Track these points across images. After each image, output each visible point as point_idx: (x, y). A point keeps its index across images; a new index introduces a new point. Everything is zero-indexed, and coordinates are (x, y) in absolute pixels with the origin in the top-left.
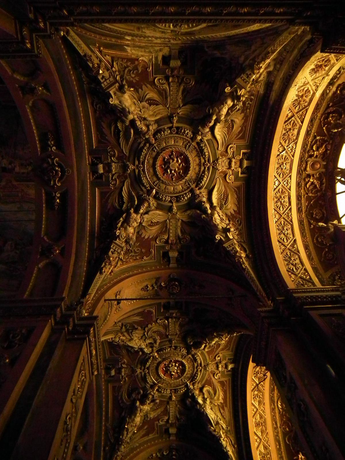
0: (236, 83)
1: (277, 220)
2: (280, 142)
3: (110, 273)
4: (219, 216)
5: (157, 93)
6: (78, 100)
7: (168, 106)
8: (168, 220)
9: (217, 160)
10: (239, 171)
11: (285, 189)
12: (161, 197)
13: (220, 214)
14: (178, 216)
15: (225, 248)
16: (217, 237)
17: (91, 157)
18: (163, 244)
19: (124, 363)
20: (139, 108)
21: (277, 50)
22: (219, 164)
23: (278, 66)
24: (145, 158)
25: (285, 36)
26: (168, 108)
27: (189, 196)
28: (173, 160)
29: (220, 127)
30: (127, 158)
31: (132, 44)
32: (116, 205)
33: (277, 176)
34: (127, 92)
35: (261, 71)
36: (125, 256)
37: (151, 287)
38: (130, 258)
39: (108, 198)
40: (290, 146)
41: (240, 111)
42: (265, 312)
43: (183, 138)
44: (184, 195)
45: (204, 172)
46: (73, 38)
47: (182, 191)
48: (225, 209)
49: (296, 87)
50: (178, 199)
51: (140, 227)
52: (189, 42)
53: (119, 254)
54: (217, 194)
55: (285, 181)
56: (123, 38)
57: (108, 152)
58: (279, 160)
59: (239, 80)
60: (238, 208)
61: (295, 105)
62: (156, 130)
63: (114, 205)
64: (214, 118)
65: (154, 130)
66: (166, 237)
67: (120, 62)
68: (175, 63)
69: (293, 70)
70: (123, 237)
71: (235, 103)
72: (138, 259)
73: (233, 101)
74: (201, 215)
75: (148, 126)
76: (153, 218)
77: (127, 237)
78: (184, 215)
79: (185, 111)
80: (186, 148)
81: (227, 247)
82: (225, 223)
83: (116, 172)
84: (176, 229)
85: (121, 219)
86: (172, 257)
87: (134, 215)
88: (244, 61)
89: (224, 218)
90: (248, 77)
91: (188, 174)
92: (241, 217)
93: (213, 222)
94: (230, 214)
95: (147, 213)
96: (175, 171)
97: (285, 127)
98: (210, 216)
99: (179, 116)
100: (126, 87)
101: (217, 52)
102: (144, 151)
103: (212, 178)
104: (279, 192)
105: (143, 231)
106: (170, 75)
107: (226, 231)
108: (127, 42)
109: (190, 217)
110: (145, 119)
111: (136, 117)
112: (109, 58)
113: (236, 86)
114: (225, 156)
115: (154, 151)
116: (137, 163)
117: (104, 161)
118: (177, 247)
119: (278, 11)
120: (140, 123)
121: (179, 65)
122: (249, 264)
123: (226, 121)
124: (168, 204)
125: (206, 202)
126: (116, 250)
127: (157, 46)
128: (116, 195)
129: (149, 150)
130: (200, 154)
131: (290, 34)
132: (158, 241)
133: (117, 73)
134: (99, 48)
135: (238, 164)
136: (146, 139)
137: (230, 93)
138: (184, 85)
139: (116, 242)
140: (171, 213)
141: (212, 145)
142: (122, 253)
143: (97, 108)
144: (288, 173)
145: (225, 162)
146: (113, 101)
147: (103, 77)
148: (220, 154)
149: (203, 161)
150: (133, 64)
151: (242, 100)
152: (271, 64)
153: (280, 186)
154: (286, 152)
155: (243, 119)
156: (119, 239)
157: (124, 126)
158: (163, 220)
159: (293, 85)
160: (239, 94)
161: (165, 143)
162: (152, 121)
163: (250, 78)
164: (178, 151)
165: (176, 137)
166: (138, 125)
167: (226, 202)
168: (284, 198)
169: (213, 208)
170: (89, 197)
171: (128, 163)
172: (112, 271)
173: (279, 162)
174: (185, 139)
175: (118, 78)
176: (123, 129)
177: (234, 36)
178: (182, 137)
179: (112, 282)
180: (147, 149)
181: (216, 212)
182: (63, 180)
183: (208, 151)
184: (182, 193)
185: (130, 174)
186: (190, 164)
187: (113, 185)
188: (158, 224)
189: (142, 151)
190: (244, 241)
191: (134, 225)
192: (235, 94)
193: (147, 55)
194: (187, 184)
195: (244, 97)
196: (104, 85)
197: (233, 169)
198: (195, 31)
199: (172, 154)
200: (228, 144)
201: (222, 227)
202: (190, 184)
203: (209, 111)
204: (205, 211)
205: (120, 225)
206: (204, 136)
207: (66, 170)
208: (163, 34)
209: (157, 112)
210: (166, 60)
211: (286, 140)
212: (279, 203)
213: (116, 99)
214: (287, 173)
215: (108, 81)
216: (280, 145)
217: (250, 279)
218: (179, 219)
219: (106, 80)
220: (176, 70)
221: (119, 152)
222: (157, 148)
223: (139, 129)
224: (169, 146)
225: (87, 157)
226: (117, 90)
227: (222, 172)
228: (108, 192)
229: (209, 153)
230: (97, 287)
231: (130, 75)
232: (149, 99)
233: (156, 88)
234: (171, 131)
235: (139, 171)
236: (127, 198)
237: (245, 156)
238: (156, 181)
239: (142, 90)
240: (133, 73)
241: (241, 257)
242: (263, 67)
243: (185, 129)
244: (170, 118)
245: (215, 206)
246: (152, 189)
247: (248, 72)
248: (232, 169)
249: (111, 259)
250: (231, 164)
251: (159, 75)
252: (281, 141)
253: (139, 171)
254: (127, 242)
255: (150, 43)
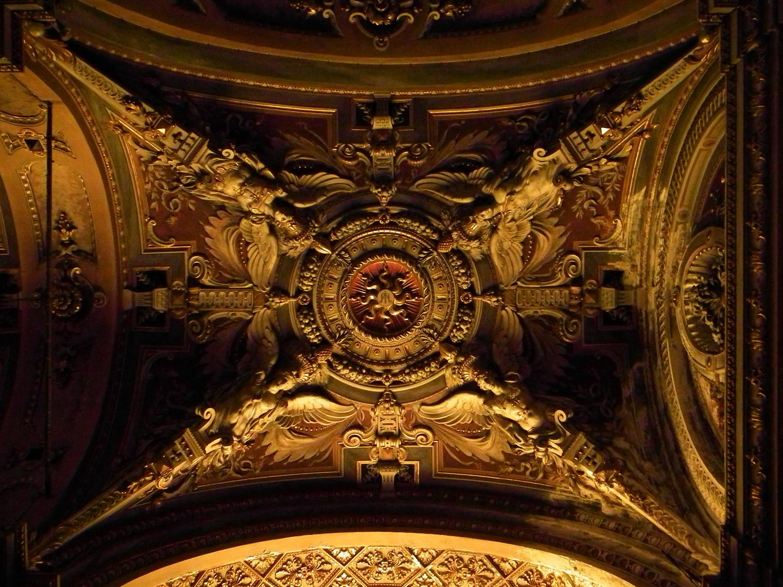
0: (574, 434)
1: (253, 564)
2: (443, 551)
3: (120, 126)
4: (262, 416)
5: (549, 260)
6: (550, 77)
7: (519, 283)
8: (250, 285)
9: (398, 404)
10: (369, 460)
11: (330, 579)
12: (311, 267)
13: (266, 418)
14: (262, 311)
15: (179, 433)
16: (208, 412)
17: (408, 102)
18: (187, 275)
19: (411, 157)
20: (520, 218)
21: (651, 515)
22: (388, 409)
23: (612, 525)
24: (407, 230)
25: (683, 528)
26: (515, 284)
27: (312, 337)
28: (398, 298)
29: (474, 406)
30: (405, 188)
31: (649, 204)
32: (295, 156)
33: (360, 556)
34: (556, 189)
35: (603, 488)
36: (164, 170)
37: (70, 238)
38: (156, 182)
39: (310, 137)
40: (434, 578)
41: (509, 450)
42: (19, 547)
43: (449, 320)
44: (314, 326)
45: (370, 372)
46: (679, 70)
47: (324, 321)
48: (278, 430)
49: (573, 569)
50: (304, 310)
51: (238, 214)
52: (651, 328)
53: (173, 154)
54: (316, 407)
55: (349, 576)
56: (663, 182)
57: (420, 141)
58: (400, 555)
59: (581, 439)
60: (279, 465)
61: (529, 575)
62: (468, 256)
63: (294, 151)
64: (497, 391)
65: (469, 252)
66: (206, 281)
67: (616, 176)
68: (608, 298)
69: (609, 559)
70: (215, 167)
71: (529, 436)
72: (150, 205)
73: (535, 431)
74: (265, 370)
75: (477, 237)
76: (258, 248)
77: (215, 176)
78: (262, 325)
79: (509, 324)
80: (425, 327)
81: (183, 440)
82: (243, 431)
83: (374, 161)
84: (227, 307)
85: (261, 166)
86: (151, 295)
87: (269, 198)
88: (618, 449)
89: (258, 429)
90: (588, 458)
91: (366, 333)
92: (258, 472)
93: (248, 399)
94: (265, 443)
95: (273, 230)
96: (373, 302)
97: (478, 558)
98: (262, 392)
99: (499, 310)
100: (568, 188)
101: (631, 387)
102: (423, 227)
103: (353, 394)
104: (323, 563)
105: (226, 221)
106: (585, 288)
107: (226, 434)
108: (653, 193)
109: (259, 341)
110: (494, 230)
111: (501, 209)
112: (626, 152)
113: (568, 433)
114: (407, 423)
115: (420, 253)
116: (394, 210)
117: (399, 132)
118: (177, 309)
119: (755, 495)
120: (487, 217)
121: (604, 309)
122: (137, 500)
123: (488, 419)
124: (293, 284)
125: (299, 380)
126: (184, 147)
127: (641, 260)
128: (317, 157)
129: (422, 240)
130: (411, 363)
131: (689, 536)
132: (196, 260)
133: (595, 169)
134: (649, 130)
135: (388, 457)
136: (449, 233)
137: (553, 423)
138: (564, 319)
139: (205, 147)
140: (269, 294)
141: (432, 389)
142: (173, 162)
143: (519, 121)
144: (369, 581)
145: (392, 424)
146: (538, 158)
147: (592, 136)
148: (411, 411)
149: (396, 369)
150: (609, 205)
151: (538, 450)
152: (616, 508)
153: (336, 565)
154: (418, 570)
155: (491, 459)
156: (211, 156)
157: (480, 182)
158: (253, 273)
159: (576, 563)
160: (553, 443)
161: (440, 278)
162: (489, 247)
163: (587, 465)
164: (418, 310)
165: (453, 304)
166: (484, 213)
167: (296, 433)
168: (307, 579)
169: (281, 399)
170: (316, 90)
171: (394, 189)
172: (125, 132)
173: (395, 556)
174: (447, 326)
175: (586, 171)
176: (471, 179)
177: (670, 421)
178: (453, 317)
179: (94, 129)
180: (425, 234)
181: (272, 407)
182: (363, 31)
183: (420, 379)
184: (319, 321)
185: (368, 192)
186: (389, 338)
187: (343, 151)
188: (241, 261)
189: (421, 224)
190: (196, 485)
191: (246, 198)
192: (551, 433)
193: (626, 237)
194: (342, 332)
195: (544, 456)
196: (575, 138)
197: (376, 445)
198: (678, 334)
199: (413, 296)
200: (435, 430)
201: (235, 424)
202: (342, 340)
203: (511, 378)
204: (275, 377)
205: (247, 160)
206: (454, 369)
207: (386, 39)
208: (671, 269)
209: (507, 258)
210: (614, 278)
211: (447, 566)
212: (294, 566)
213: (542, 163)
214: (368, 578)
215: (583, 146)
216: (434, 554)
217: (98, 505)
218: (254, 314)
219: (585, 141)
220: (594, 302)
221: (419, 169)
222: (428, 258)
223: (472, 214)
224: (432, 288)
225: (409, 93)
226: (562, 165)
227: (369, 418)
228: (326, 139)
229: (414, 383)
230: (88, 83)
231: (588, 199)
232: (535, 239)
233: (557, 256)
234: (466, 290)
235: (375, 215)
236: (311, 183)
237: (406, 471)
238: (350, 256)
239: (556, 225)
240: (592, 205)
241: (156, 477)
242: (611, 490)
243: (470, 323)
244: (494, 289)
245: (286, 405)
246: (332, 245)
247: (598, 460)
248: (377, 443)
249: (163, 131)
250: (388, 439)
251: (585, 262)
252: (444, 554)
253: (375, 215)
254: (202, 176)
255: (649, 244)
